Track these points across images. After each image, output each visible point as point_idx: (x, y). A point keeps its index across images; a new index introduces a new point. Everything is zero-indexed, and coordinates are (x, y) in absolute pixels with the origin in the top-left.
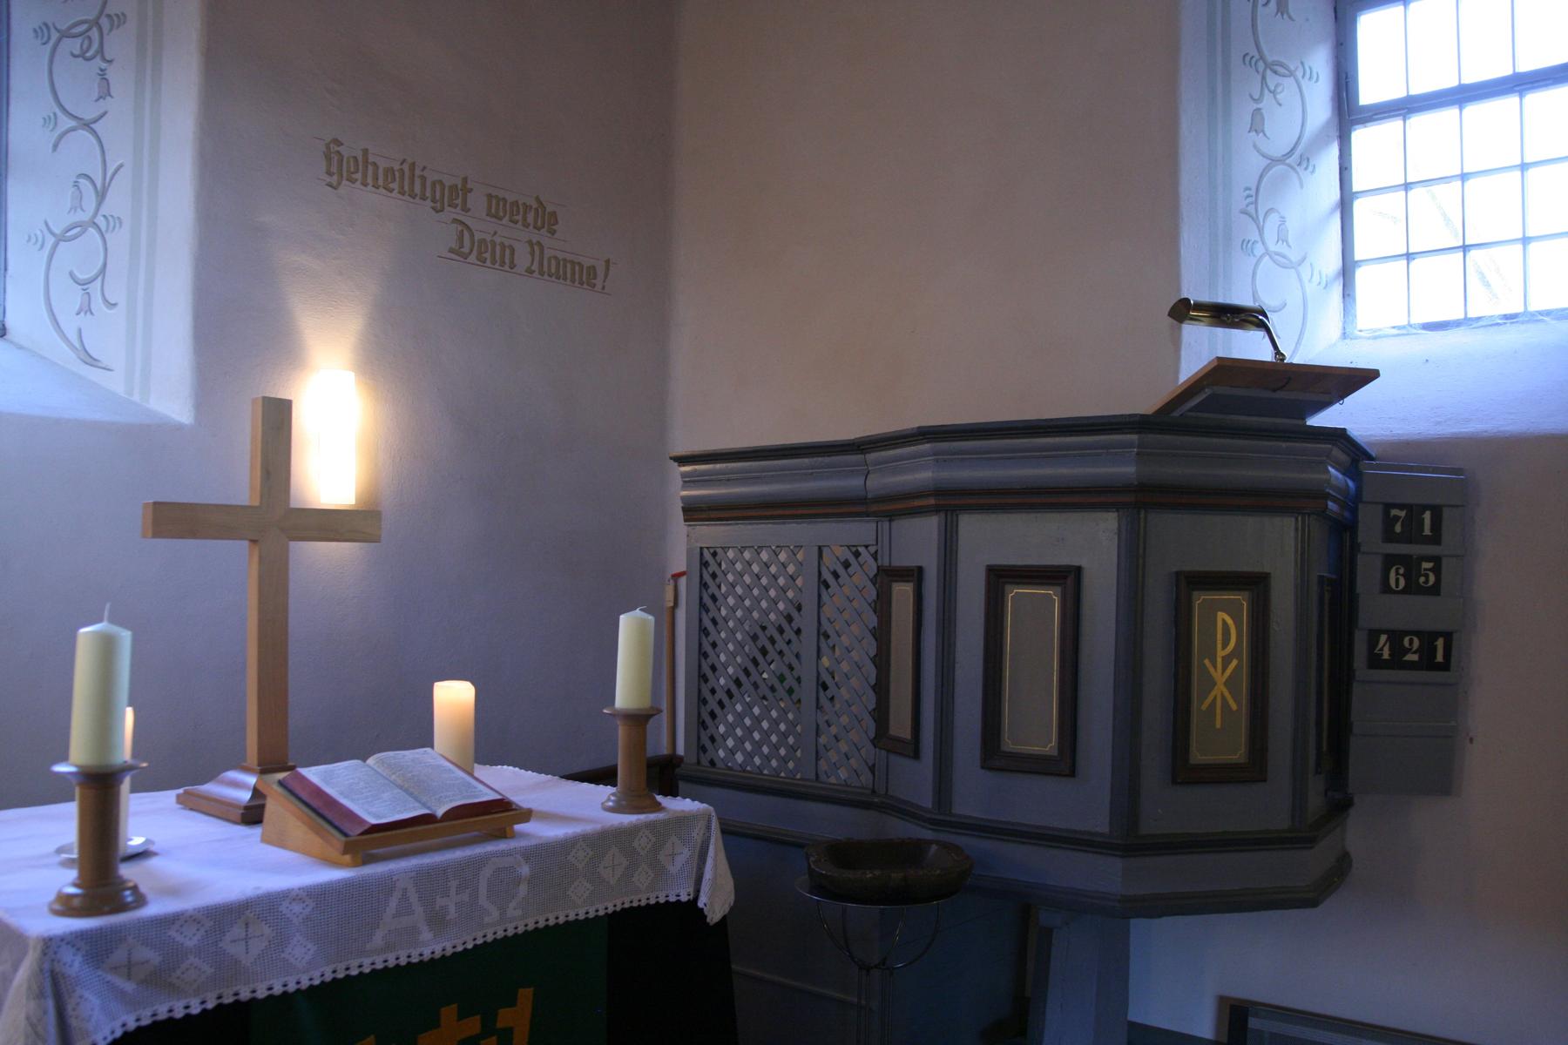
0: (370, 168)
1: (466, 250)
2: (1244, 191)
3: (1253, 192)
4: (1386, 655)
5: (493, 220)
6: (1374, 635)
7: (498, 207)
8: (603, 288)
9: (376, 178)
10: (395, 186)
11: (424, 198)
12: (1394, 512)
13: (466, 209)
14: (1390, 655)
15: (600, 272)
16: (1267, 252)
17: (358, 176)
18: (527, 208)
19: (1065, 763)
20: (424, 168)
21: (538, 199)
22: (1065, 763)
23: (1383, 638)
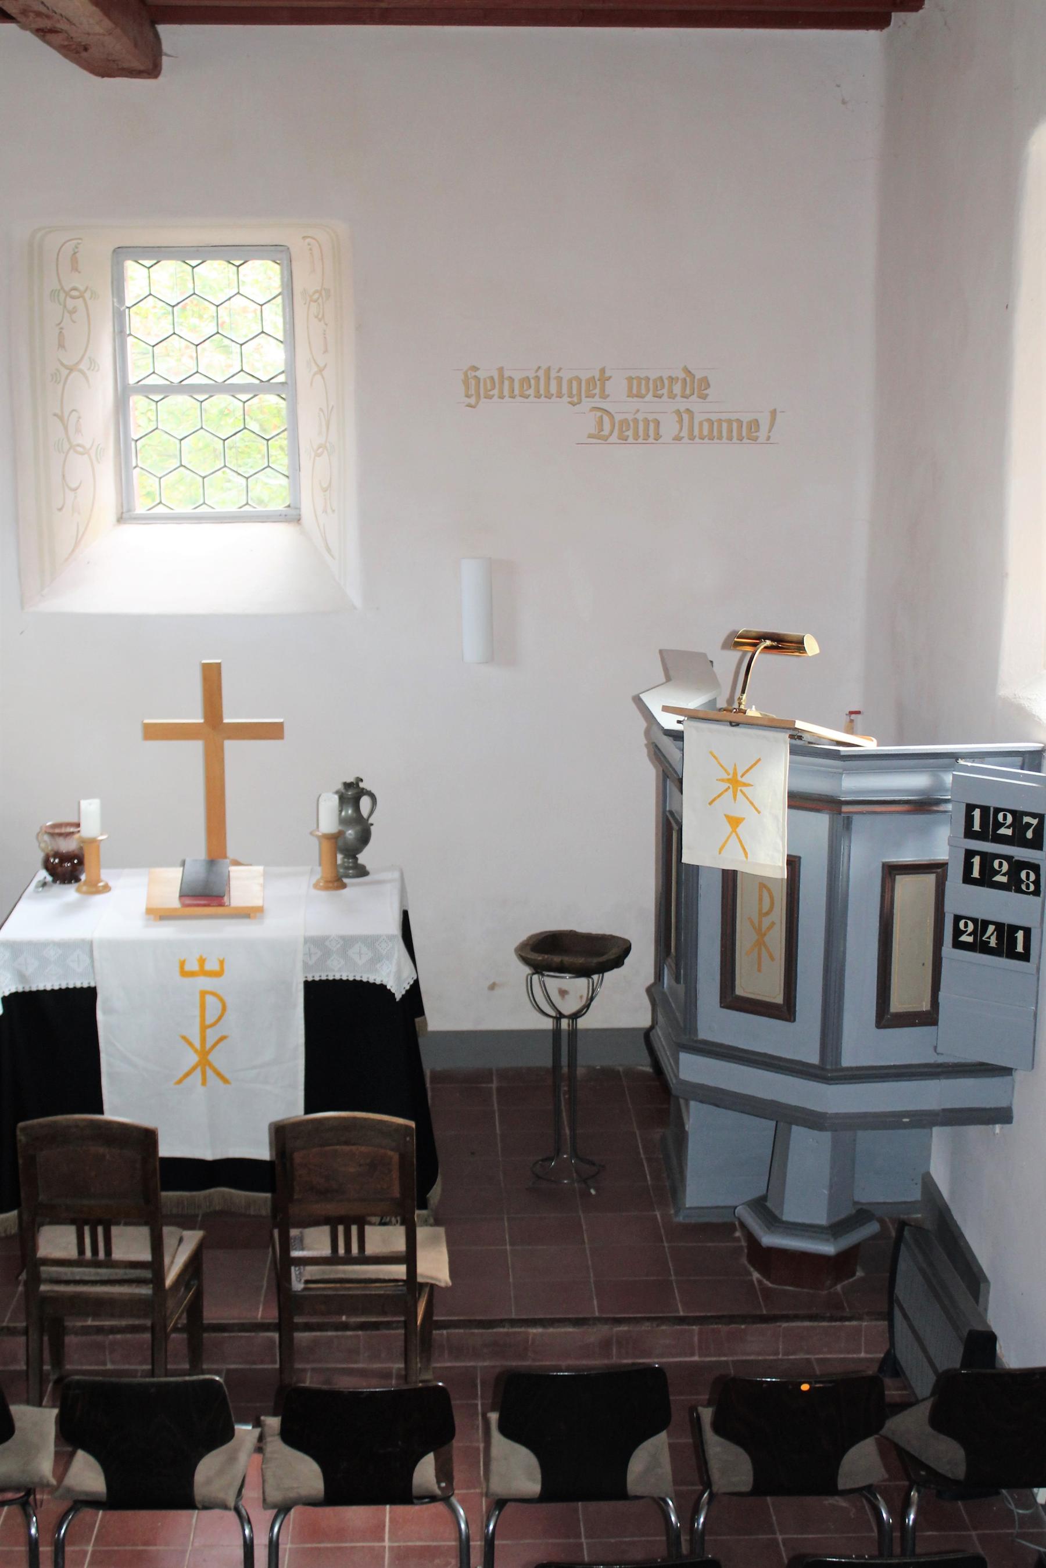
0: (506, 383)
4: (993, 943)
5: (635, 399)
6: (957, 918)
7: (637, 387)
8: (769, 438)
9: (512, 390)
11: (560, 395)
12: (1027, 819)
13: (604, 396)
14: (996, 944)
17: (496, 392)
18: (671, 379)
19: (786, 1011)
22: (786, 1011)
23: (991, 928)
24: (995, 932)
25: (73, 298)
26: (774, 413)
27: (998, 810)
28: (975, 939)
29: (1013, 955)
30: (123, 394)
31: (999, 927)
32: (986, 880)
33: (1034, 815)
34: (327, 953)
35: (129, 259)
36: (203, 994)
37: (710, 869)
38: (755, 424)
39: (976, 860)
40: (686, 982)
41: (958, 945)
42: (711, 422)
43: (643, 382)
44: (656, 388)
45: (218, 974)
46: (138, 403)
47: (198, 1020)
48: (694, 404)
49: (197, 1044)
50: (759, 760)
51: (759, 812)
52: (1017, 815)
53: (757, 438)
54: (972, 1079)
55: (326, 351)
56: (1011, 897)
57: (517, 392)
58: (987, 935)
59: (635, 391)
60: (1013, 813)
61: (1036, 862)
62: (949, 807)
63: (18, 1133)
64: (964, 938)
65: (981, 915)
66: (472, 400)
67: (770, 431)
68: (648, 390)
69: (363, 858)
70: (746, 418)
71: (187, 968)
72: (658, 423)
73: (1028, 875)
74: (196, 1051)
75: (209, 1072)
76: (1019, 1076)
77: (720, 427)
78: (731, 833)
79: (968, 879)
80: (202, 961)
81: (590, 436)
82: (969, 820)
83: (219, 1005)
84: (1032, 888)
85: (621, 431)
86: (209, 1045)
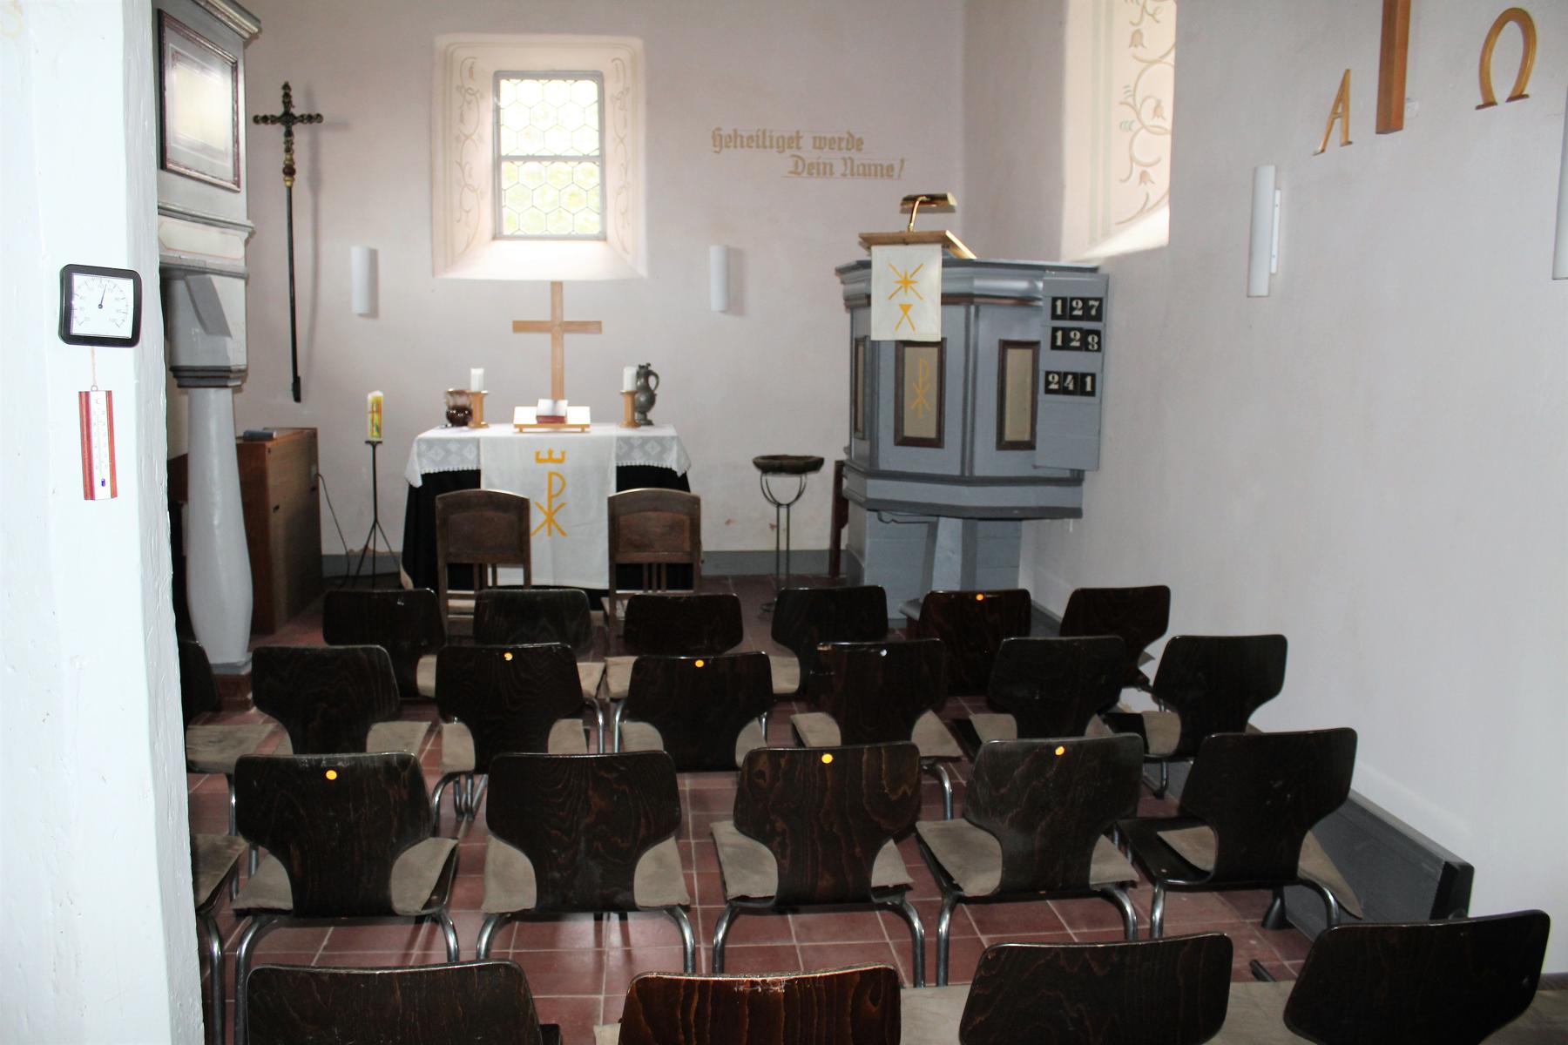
0: (739, 139)
3: (1131, 88)
4: (1071, 387)
6: (1048, 373)
7: (819, 143)
8: (899, 176)
9: (742, 142)
11: (771, 147)
12: (1091, 303)
13: (798, 148)
16: (1144, 126)
17: (732, 144)
18: (840, 139)
19: (936, 442)
23: (1070, 377)
26: (903, 161)
27: (1072, 299)
29: (1084, 393)
30: (498, 161)
31: (1075, 375)
32: (1066, 346)
33: (1095, 299)
36: (551, 474)
38: (891, 168)
39: (1059, 334)
41: (1048, 391)
42: (864, 166)
45: (560, 461)
46: (505, 165)
47: (546, 492)
49: (546, 508)
52: (1085, 300)
53: (892, 176)
55: (626, 126)
56: (1082, 355)
57: (745, 144)
60: (1083, 299)
61: (1098, 329)
62: (1040, 303)
63: (437, 502)
64: (1054, 387)
65: (1063, 369)
68: (825, 144)
69: (651, 415)
71: (541, 457)
72: (831, 165)
74: (545, 513)
75: (553, 526)
77: (870, 169)
78: (903, 317)
79: (1054, 347)
80: (550, 452)
81: (791, 172)
84: (1096, 347)
85: (809, 170)
86: (553, 508)
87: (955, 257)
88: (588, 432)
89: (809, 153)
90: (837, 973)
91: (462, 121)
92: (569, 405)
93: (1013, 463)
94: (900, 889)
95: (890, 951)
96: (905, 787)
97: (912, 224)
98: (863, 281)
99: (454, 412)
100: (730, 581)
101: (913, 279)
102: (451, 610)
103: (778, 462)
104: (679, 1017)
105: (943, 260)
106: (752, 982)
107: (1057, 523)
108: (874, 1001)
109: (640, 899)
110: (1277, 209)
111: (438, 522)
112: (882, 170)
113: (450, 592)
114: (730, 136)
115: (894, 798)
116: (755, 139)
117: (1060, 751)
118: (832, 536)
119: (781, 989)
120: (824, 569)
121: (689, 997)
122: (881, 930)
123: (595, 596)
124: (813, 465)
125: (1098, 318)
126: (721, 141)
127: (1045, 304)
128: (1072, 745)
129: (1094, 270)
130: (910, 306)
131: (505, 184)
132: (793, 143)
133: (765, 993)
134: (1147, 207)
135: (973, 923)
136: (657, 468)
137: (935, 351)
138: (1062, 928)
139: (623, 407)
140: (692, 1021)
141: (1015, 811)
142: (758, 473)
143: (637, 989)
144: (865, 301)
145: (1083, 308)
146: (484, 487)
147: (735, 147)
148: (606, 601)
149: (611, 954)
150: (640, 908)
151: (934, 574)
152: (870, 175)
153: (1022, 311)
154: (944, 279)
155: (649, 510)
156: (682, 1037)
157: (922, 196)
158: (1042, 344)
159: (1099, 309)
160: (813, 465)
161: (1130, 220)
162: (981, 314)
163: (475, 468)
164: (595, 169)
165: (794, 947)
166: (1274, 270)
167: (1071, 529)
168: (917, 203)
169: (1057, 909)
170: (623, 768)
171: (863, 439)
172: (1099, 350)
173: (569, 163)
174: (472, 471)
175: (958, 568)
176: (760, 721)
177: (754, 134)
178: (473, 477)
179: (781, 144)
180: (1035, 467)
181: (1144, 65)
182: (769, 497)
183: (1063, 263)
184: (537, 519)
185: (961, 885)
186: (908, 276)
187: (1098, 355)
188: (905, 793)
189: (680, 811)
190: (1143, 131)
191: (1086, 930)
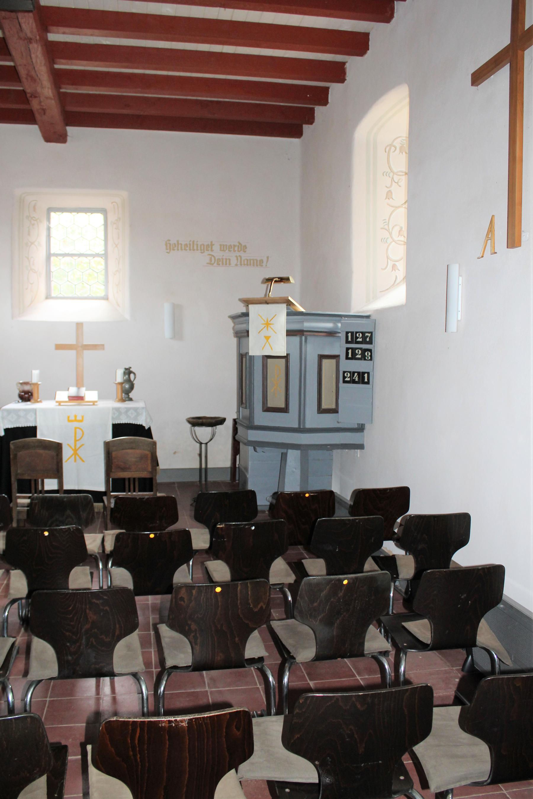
0: (180, 245)
1: (213, 262)
2: (383, 221)
3: (387, 221)
4: (357, 379)
5: (222, 252)
6: (344, 372)
7: (223, 248)
8: (266, 265)
9: (181, 247)
10: (188, 248)
11: (197, 250)
12: (367, 334)
13: (212, 250)
15: (265, 260)
16: (394, 241)
17: (176, 248)
18: (234, 246)
19: (285, 410)
20: (197, 241)
21: (239, 243)
23: (356, 374)
24: (357, 376)
25: (34, 220)
26: (268, 257)
27: (357, 333)
28: (350, 379)
29: (364, 382)
30: (49, 256)
31: (359, 373)
32: (354, 357)
33: (369, 333)
34: (120, 413)
35: (52, 212)
37: (259, 356)
38: (261, 261)
39: (350, 351)
40: (250, 408)
41: (345, 382)
42: (247, 260)
43: (225, 246)
44: (229, 248)
45: (81, 421)
46: (53, 259)
48: (242, 254)
49: (73, 446)
50: (276, 315)
51: (276, 333)
52: (363, 333)
54: (351, 433)
57: (183, 248)
58: (354, 377)
59: (222, 249)
60: (362, 333)
61: (371, 348)
62: (340, 335)
64: (347, 379)
65: (352, 370)
66: (168, 251)
67: (267, 263)
69: (131, 395)
70: (259, 259)
72: (230, 260)
73: (368, 353)
74: (73, 450)
75: (77, 457)
76: (367, 427)
78: (267, 342)
79: (347, 358)
80: (76, 416)
82: (347, 337)
83: (81, 432)
84: (369, 358)
87: (293, 310)
88: (97, 405)
89: (217, 253)
90: (216, 714)
91: (29, 234)
92: (86, 390)
93: (327, 421)
94: (261, 659)
95: (260, 692)
96: (261, 604)
97: (270, 293)
98: (245, 323)
99: (23, 394)
100: (176, 485)
101: (272, 322)
102: (19, 505)
103: (201, 420)
104: (129, 741)
105: (287, 312)
106: (169, 721)
107: (352, 451)
108: (238, 729)
109: (116, 670)
110: (460, 287)
111: (11, 456)
112: (257, 262)
113: (18, 495)
114: (175, 244)
115: (256, 610)
116: (188, 245)
117: (345, 582)
118: (231, 460)
119: (186, 724)
120: (227, 478)
121: (134, 731)
122: (255, 680)
123: (98, 496)
124: (221, 421)
125: (371, 342)
126: (170, 247)
127: (343, 336)
128: (352, 578)
129: (368, 317)
130: (269, 337)
131: (53, 269)
132: (209, 247)
133: (176, 727)
134: (396, 284)
135: (306, 675)
136: (135, 424)
137: (283, 361)
138: (354, 676)
139: (115, 391)
140: (137, 744)
141: (322, 615)
142: (189, 426)
143: (105, 726)
144: (246, 334)
145: (362, 337)
146: (39, 437)
147: (178, 250)
148: (105, 498)
149: (105, 699)
150: (117, 675)
151: (286, 480)
152: (250, 265)
153: (330, 339)
154: (288, 322)
155: (128, 449)
156: (131, 753)
157: (276, 278)
158: (341, 357)
159: (371, 338)
160: (221, 421)
161: (387, 290)
162: (308, 341)
163: (34, 425)
164: (102, 261)
165: (207, 691)
166: (459, 319)
167: (359, 456)
168: (273, 282)
169: (350, 665)
170: (105, 597)
171: (246, 408)
172: (371, 359)
173: (88, 258)
174: (33, 427)
175: (298, 478)
176: (188, 565)
177: (188, 243)
178: (32, 431)
179: (202, 248)
180: (338, 422)
181: (394, 208)
182: (197, 440)
183: (352, 313)
184: (66, 453)
185: (295, 656)
186: (269, 321)
187: (371, 362)
188: (262, 607)
189: (138, 620)
190: (394, 243)
191: (367, 677)
